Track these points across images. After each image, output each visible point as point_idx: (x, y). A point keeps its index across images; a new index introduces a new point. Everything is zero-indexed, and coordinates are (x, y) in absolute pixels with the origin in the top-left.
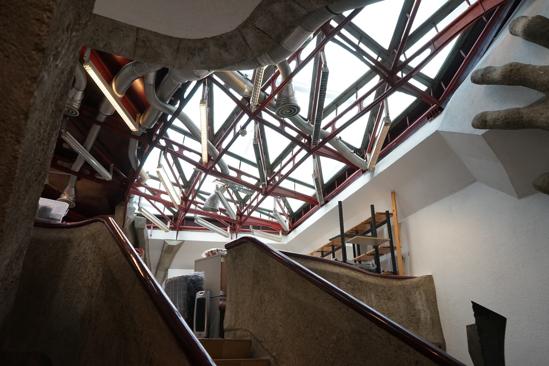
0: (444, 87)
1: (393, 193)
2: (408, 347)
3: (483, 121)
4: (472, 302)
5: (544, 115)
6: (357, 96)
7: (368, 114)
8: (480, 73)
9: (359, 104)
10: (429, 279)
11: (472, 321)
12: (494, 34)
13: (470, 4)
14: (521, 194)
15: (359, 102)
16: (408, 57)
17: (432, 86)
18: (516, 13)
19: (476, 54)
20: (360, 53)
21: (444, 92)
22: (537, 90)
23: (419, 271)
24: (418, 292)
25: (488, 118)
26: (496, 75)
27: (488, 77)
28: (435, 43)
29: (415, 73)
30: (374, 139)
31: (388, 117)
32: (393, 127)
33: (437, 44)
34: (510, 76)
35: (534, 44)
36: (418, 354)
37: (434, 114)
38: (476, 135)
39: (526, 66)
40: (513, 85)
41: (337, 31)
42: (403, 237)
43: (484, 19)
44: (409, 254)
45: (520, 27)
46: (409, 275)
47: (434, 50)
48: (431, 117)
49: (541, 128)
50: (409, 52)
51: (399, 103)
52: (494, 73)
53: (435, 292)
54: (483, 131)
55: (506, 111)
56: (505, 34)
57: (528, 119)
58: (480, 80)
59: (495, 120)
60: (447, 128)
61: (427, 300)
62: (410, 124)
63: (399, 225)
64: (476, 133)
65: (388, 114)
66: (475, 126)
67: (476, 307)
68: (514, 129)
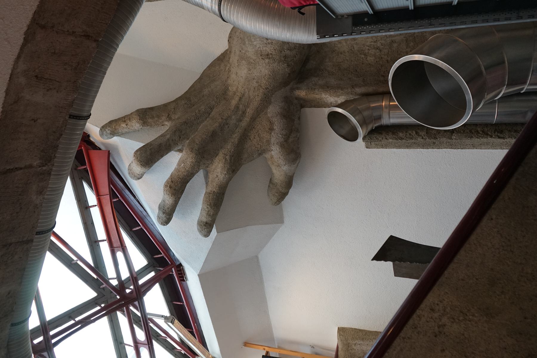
0: (159, 256)
1: (246, 344)
2: (414, 316)
3: (205, 225)
4: (373, 260)
5: (219, 174)
6: (130, 345)
7: (155, 343)
8: (161, 215)
9: (139, 345)
10: (342, 331)
11: (389, 265)
12: (132, 198)
13: (96, 206)
14: (280, 220)
15: (137, 345)
16: (115, 276)
17: (154, 267)
18: (124, 175)
19: (143, 219)
20: (86, 322)
21: (165, 257)
22: (195, 173)
23: (332, 341)
24: (353, 346)
25: (205, 220)
26: (169, 201)
27: (168, 208)
28: (115, 245)
29: (134, 277)
30: (182, 343)
31: (166, 318)
32: (176, 315)
33: (116, 243)
34: (175, 190)
35: (156, 164)
36: (423, 306)
37: (181, 274)
38: (215, 239)
39: (171, 175)
40: (183, 191)
41: (47, 339)
42: (294, 348)
43: (115, 200)
44: (313, 347)
45: (137, 169)
46: (334, 353)
47: (121, 249)
48: (183, 277)
49: (229, 181)
50: (111, 273)
51: (155, 302)
52: (167, 202)
53: (355, 329)
54: (214, 230)
55: (203, 203)
56: (136, 185)
57: (218, 188)
58: (167, 217)
59: (208, 214)
60: (199, 265)
61: (363, 340)
62: (183, 303)
63: (279, 348)
64: (214, 238)
65: (162, 316)
66: (207, 235)
67: (377, 258)
68: (222, 202)
